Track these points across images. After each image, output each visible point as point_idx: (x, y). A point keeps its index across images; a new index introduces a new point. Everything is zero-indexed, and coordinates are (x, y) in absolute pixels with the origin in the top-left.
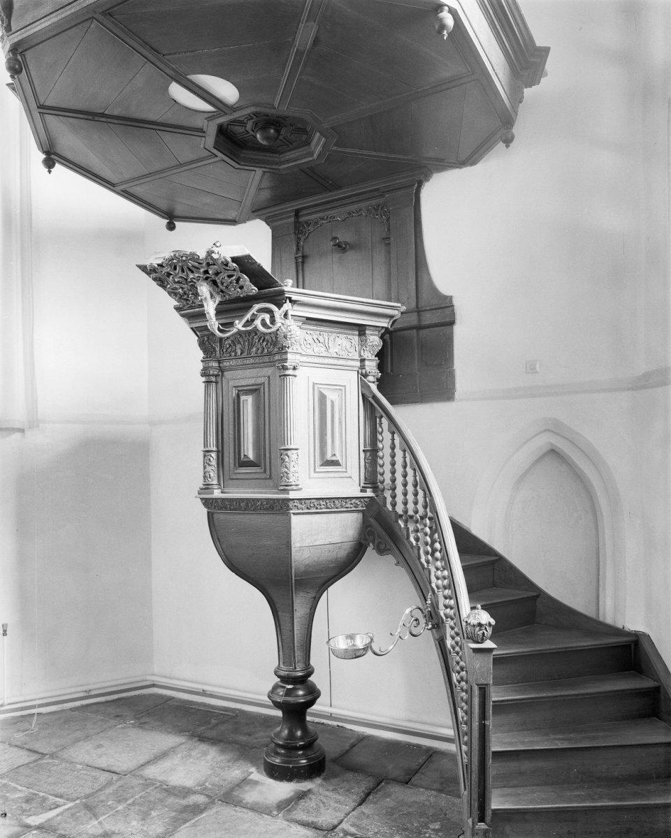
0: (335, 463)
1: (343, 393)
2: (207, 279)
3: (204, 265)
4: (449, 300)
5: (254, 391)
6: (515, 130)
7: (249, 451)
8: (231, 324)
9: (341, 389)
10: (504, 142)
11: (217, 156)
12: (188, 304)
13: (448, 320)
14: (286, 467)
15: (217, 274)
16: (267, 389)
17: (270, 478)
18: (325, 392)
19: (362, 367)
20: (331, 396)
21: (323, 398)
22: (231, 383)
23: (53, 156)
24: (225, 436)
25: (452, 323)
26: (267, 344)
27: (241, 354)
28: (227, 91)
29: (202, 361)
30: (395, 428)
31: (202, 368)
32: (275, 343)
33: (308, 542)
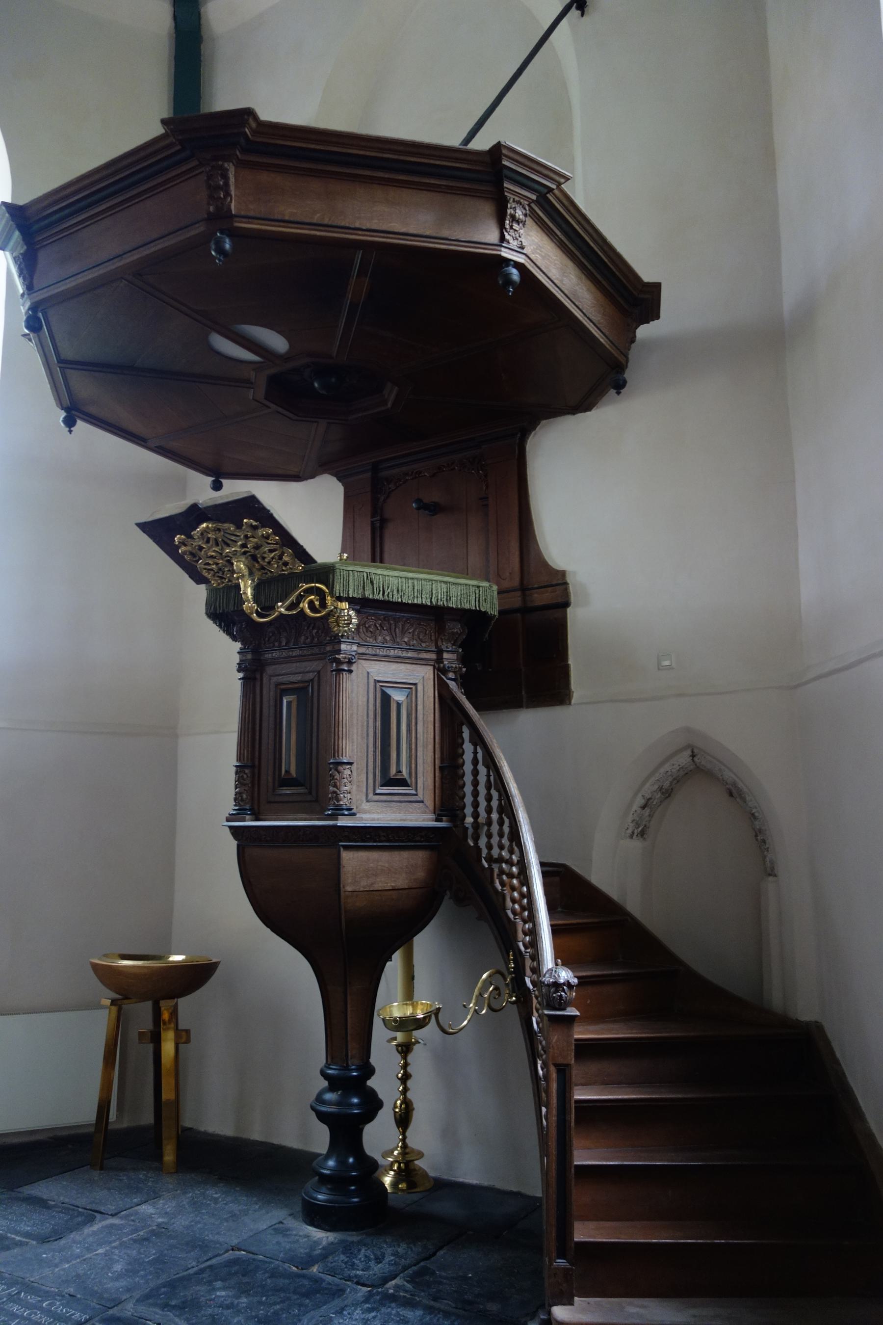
0: (403, 783)
1: (414, 692)
2: (245, 553)
3: (242, 537)
4: (563, 573)
5: (300, 690)
6: (627, 375)
7: (290, 764)
8: (272, 608)
9: (411, 688)
10: (615, 388)
11: (269, 408)
12: (223, 583)
13: (560, 600)
14: (335, 786)
15: (257, 547)
16: (316, 687)
17: (317, 801)
18: (389, 691)
19: (440, 660)
20: (398, 696)
21: (386, 699)
22: (274, 679)
23: (74, 412)
24: (264, 748)
25: (566, 604)
26: (317, 632)
27: (286, 643)
28: (277, 342)
29: (238, 653)
30: (478, 739)
31: (238, 661)
32: (327, 630)
33: (364, 884)
